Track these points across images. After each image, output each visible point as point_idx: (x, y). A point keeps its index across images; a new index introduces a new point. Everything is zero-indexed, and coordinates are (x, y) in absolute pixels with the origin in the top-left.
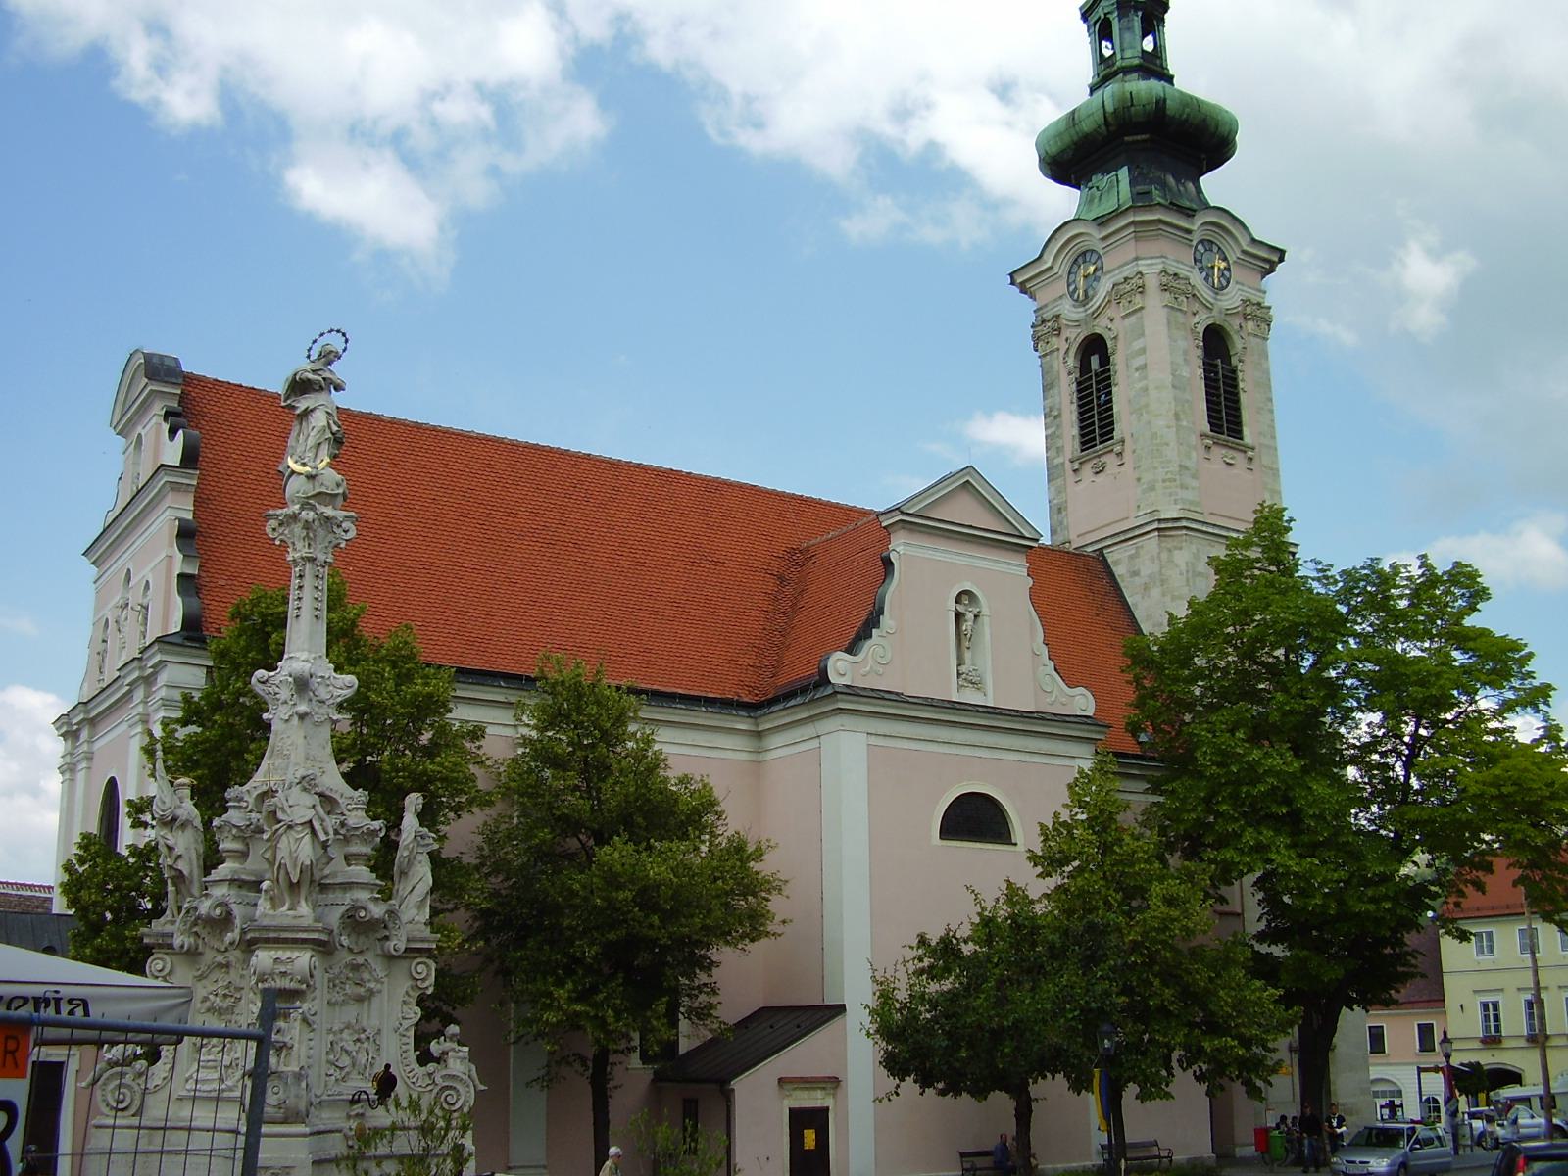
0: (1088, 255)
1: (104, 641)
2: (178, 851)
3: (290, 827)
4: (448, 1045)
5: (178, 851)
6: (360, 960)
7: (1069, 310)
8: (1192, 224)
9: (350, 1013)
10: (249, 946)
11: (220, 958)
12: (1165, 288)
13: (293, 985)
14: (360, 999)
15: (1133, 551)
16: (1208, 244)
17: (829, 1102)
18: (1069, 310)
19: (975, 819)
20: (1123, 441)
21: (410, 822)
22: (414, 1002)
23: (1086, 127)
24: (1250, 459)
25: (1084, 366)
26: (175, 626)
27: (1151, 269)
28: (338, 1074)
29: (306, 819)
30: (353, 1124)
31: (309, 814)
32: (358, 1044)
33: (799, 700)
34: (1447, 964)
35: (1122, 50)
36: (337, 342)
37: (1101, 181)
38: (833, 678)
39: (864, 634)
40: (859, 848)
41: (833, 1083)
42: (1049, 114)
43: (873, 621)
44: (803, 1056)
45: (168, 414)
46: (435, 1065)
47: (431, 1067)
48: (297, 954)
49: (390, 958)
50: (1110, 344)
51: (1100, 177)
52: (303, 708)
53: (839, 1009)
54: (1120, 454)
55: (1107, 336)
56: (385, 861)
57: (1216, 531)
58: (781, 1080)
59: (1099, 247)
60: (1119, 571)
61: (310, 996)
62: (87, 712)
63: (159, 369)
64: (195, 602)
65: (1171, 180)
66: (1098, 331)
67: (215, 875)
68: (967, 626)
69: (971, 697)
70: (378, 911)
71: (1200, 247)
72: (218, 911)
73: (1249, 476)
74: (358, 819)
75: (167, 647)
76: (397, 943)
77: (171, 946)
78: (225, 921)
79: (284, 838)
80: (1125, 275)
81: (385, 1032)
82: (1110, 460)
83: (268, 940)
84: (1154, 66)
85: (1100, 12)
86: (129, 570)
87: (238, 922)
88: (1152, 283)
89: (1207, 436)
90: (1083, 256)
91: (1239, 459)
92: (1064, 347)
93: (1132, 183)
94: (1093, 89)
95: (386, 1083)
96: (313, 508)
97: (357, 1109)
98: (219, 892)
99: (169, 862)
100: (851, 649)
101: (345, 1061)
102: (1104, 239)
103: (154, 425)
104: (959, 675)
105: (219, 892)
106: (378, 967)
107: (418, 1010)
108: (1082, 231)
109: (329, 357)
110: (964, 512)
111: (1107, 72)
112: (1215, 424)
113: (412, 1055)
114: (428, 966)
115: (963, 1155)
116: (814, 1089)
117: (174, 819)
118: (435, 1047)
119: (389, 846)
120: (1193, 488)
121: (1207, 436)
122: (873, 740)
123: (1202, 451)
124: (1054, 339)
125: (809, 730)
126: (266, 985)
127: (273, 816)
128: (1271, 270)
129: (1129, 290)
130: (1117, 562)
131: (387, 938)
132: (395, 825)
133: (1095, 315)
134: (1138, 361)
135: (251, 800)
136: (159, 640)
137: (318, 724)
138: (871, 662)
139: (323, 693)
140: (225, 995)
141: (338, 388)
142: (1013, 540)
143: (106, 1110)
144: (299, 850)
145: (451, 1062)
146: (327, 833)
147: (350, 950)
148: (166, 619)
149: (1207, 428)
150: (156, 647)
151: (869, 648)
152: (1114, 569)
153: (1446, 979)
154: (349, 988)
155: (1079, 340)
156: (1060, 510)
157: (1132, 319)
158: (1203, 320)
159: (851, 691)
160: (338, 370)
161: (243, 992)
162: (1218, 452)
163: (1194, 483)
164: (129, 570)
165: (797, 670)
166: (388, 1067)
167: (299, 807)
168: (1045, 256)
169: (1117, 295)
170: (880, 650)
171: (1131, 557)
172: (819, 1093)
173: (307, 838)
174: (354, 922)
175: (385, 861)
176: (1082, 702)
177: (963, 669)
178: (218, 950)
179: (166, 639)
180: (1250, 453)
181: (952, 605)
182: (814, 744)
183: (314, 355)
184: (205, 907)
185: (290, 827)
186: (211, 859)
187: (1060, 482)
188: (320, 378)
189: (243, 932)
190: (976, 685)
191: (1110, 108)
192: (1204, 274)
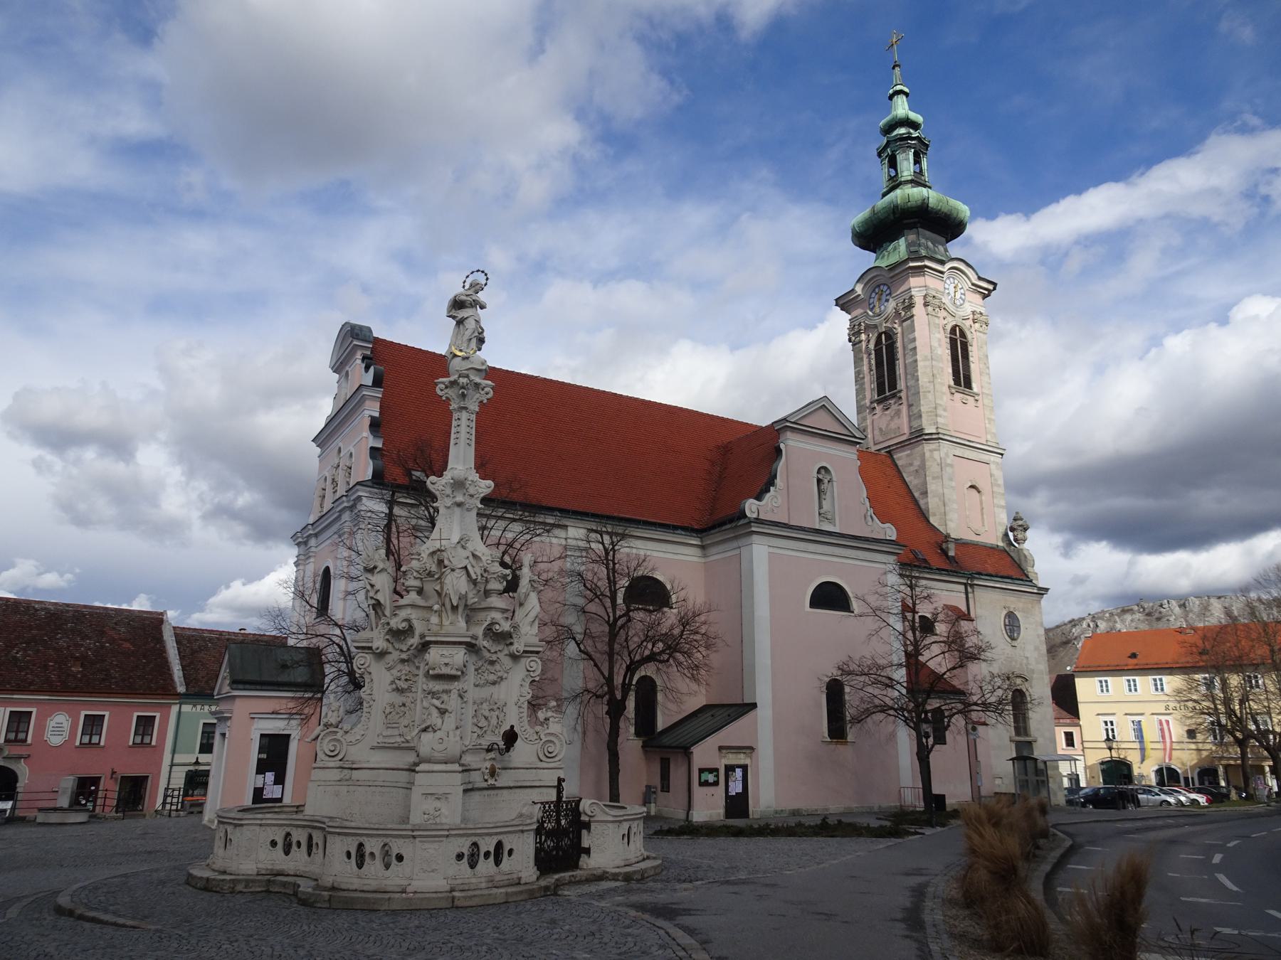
2: (377, 587)
3: (453, 570)
4: (550, 714)
5: (377, 587)
6: (494, 657)
9: (486, 692)
13: (454, 672)
19: (830, 597)
26: (369, 475)
28: (479, 731)
30: (488, 764)
33: (728, 526)
34: (1081, 696)
36: (481, 279)
38: (748, 514)
43: (771, 482)
44: (732, 733)
45: (364, 358)
49: (515, 657)
52: (460, 498)
53: (753, 706)
60: (900, 463)
64: (379, 462)
69: (827, 527)
70: (505, 626)
76: (518, 646)
78: (410, 630)
87: (417, 633)
96: (467, 376)
97: (492, 755)
101: (483, 723)
105: (403, 614)
106: (507, 662)
109: (476, 287)
110: (821, 421)
112: (957, 382)
118: (541, 715)
122: (771, 550)
125: (735, 544)
127: (440, 562)
128: (988, 295)
130: (900, 459)
131: (511, 644)
134: (911, 346)
137: (469, 510)
141: (482, 307)
142: (847, 438)
144: (456, 584)
149: (952, 383)
153: (1080, 706)
159: (758, 521)
160: (482, 296)
162: (958, 396)
166: (512, 727)
167: (458, 558)
172: (742, 756)
174: (490, 632)
176: (890, 532)
181: (815, 474)
182: (737, 552)
183: (467, 286)
190: (831, 521)
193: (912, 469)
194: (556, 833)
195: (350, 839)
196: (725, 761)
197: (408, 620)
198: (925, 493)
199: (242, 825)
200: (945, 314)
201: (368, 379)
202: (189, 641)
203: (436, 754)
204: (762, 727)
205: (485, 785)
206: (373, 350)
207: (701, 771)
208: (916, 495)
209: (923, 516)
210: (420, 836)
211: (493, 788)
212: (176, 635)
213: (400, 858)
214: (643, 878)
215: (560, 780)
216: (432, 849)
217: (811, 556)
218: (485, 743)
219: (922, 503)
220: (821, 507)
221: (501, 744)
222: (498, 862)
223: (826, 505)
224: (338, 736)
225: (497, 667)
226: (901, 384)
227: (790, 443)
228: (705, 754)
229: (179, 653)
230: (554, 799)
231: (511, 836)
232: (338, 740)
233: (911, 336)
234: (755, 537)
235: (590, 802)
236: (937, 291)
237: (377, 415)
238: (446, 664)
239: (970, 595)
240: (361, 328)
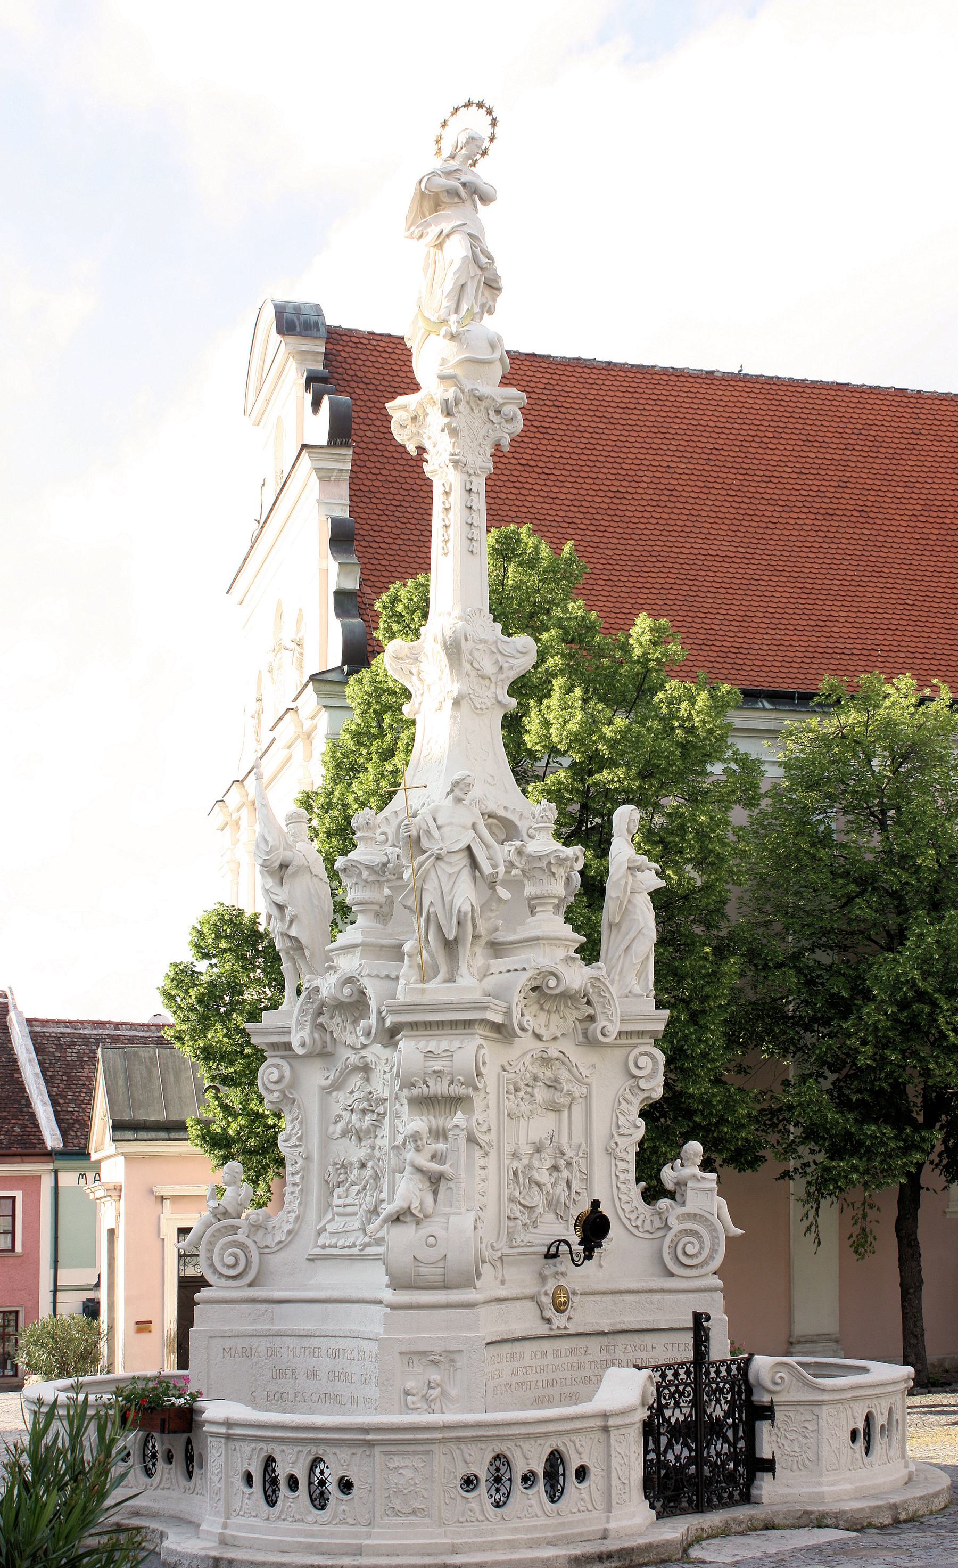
1: (259, 700)
3: (439, 858)
10: (391, 1035)
21: (622, 850)
22: (635, 1110)
26: (335, 658)
29: (462, 845)
30: (550, 1287)
31: (468, 838)
32: (555, 1174)
36: (477, 122)
46: (667, 1201)
47: (664, 1203)
48: (456, 1044)
63: (293, 322)
72: (347, 991)
74: (545, 844)
77: (288, 1046)
78: (356, 1006)
79: (432, 874)
83: (414, 1026)
95: (594, 1228)
98: (348, 964)
107: (641, 1123)
109: (475, 150)
113: (635, 1191)
114: (653, 1057)
115: (137, 1323)
119: (593, 888)
126: (415, 1091)
140: (364, 1112)
141: (486, 199)
145: (690, 1194)
161: (387, 1104)
166: (596, 1204)
173: (466, 875)
178: (353, 1048)
184: (327, 985)
185: (439, 858)
188: (457, 184)
194: (696, 1431)
195: (247, 1448)
199: (820, 1403)
202: (60, 1047)
203: (424, 1270)
205: (543, 1329)
206: (328, 357)
210: (382, 1443)
212: (34, 1036)
213: (346, 1486)
214: (897, 1522)
215: (699, 1319)
216: (407, 1470)
221: (574, 1239)
222: (554, 1491)
224: (241, 1237)
229: (44, 1071)
230: (689, 1355)
238: (438, 1074)
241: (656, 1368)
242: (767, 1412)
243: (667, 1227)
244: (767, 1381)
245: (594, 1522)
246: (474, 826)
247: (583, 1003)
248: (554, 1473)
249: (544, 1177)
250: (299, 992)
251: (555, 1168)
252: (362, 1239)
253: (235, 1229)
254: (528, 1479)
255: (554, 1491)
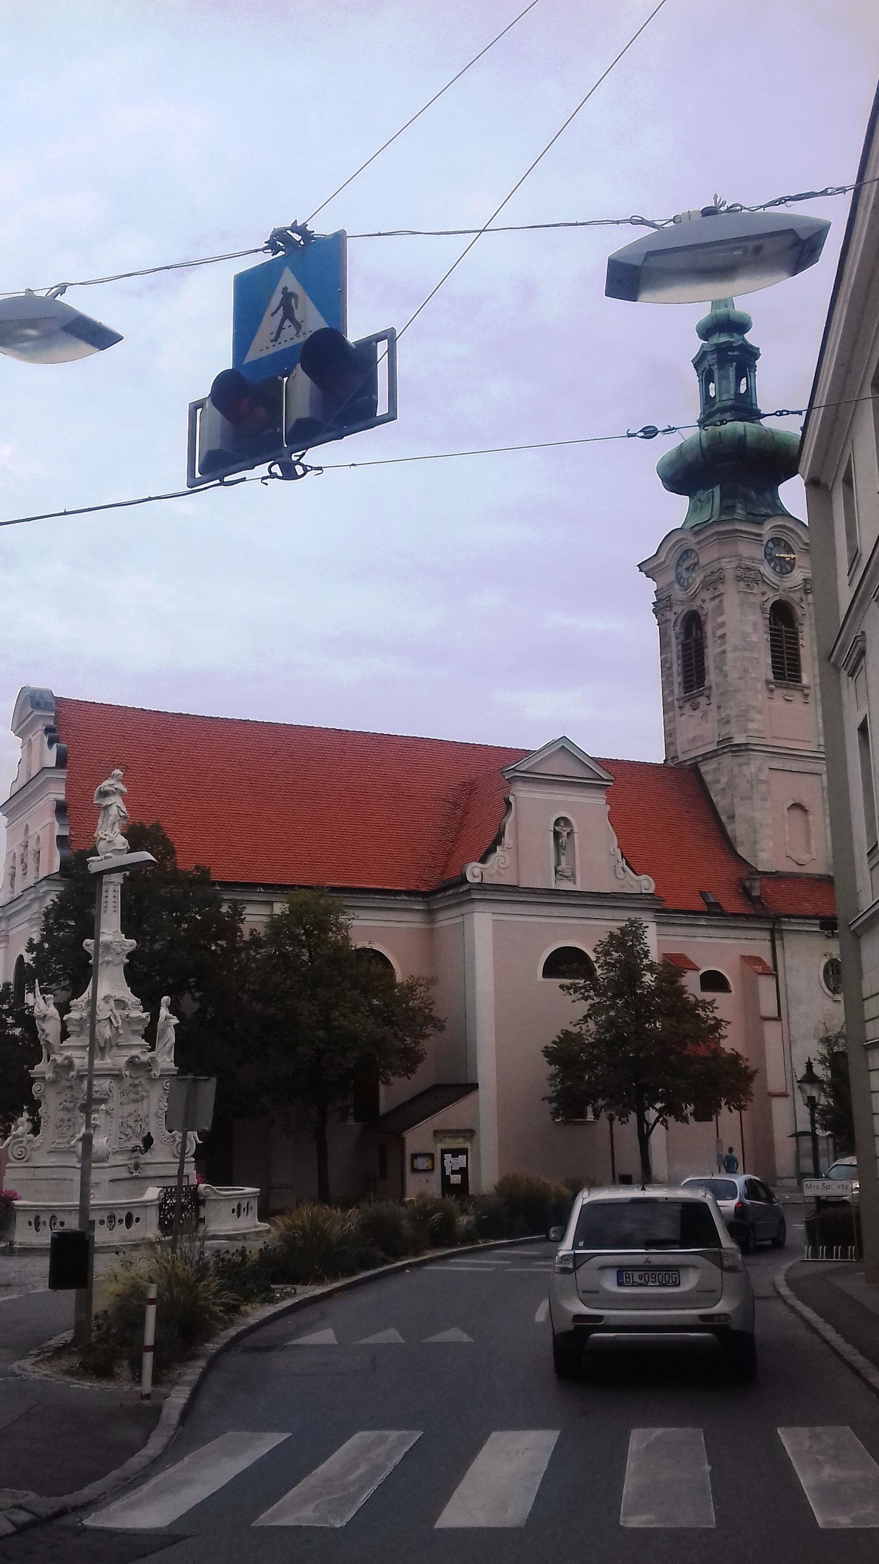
0: (689, 553)
6: (137, 1082)
7: (679, 594)
8: (763, 529)
9: (130, 1108)
11: (68, 1084)
12: (739, 579)
14: (136, 1101)
15: (716, 766)
16: (776, 541)
17: (468, 1145)
18: (679, 594)
20: (710, 688)
21: (164, 1012)
23: (689, 458)
24: (806, 696)
25: (687, 632)
27: (729, 566)
30: (132, 1162)
31: (109, 1014)
35: (720, 395)
37: (702, 495)
38: (469, 878)
39: (492, 850)
40: (499, 984)
41: (470, 1134)
42: (665, 447)
43: (498, 840)
44: (452, 1115)
45: (48, 730)
50: (703, 618)
51: (701, 492)
54: (708, 697)
55: (701, 612)
56: (151, 1035)
57: (776, 750)
58: (436, 1133)
59: (695, 548)
60: (708, 778)
61: (110, 1100)
62: (5, 912)
64: (64, 851)
65: (753, 494)
66: (695, 608)
67: (65, 1043)
68: (563, 840)
70: (145, 1058)
71: (771, 545)
73: (805, 708)
75: (50, 882)
77: (44, 1078)
80: (712, 569)
81: (150, 1117)
82: (702, 700)
84: (745, 408)
85: (705, 364)
86: (27, 826)
88: (729, 575)
89: (772, 683)
90: (687, 553)
91: (797, 696)
92: (673, 618)
93: (722, 499)
94: (702, 423)
97: (135, 1155)
99: (43, 1037)
100: (483, 860)
102: (698, 543)
103: (39, 737)
104: (556, 872)
108: (680, 537)
110: (562, 767)
111: (711, 412)
116: (458, 1137)
117: (45, 1016)
120: (759, 721)
121: (772, 683)
122: (497, 917)
123: (767, 694)
124: (668, 613)
129: (714, 581)
132: (155, 1016)
133: (694, 596)
134: (719, 632)
135: (83, 1004)
136: (45, 878)
138: (496, 867)
139: (119, 950)
143: (13, 1159)
146: (117, 1022)
147: (131, 1077)
148: (50, 866)
149: (771, 676)
150: (44, 883)
151: (493, 859)
152: (705, 777)
154: (132, 1096)
155: (683, 615)
156: (671, 735)
157: (717, 601)
158: (772, 597)
159: (482, 886)
162: (779, 693)
163: (760, 717)
164: (27, 826)
165: (452, 874)
166: (149, 1133)
168: (661, 552)
169: (706, 585)
170: (502, 860)
171: (715, 770)
172: (461, 1140)
173: (108, 1027)
175: (151, 1035)
176: (646, 884)
177: (559, 868)
179: (51, 877)
180: (806, 691)
186: (65, 1035)
187: (671, 714)
189: (79, 1071)
190: (572, 878)
191: (705, 445)
192: (773, 564)
193: (719, 786)
196: (440, 1146)
197: (67, 1058)
198: (732, 817)
200: (765, 588)
201: (51, 758)
204: (485, 1108)
207: (414, 1156)
208: (724, 818)
209: (727, 844)
211: (136, 1178)
217: (546, 920)
218: (130, 1145)
219: (729, 828)
220: (558, 863)
222: (128, 1225)
223: (563, 865)
224: (24, 1144)
225: (140, 1089)
226: (712, 678)
227: (521, 794)
228: (418, 1138)
231: (138, 1210)
232: (24, 1148)
233: (720, 620)
234: (478, 906)
235: (205, 1185)
236: (753, 560)
237: (62, 797)
239: (778, 943)
240: (42, 692)
241: (164, 1188)
242: (203, 1203)
243: (175, 1140)
244: (203, 1192)
245: (141, 1235)
246: (111, 1010)
247: (148, 1066)
248: (129, 1221)
249: (132, 1124)
250: (49, 1060)
251: (136, 1121)
252: (68, 1146)
253: (22, 1142)
254: (121, 1221)
255: (128, 1225)
